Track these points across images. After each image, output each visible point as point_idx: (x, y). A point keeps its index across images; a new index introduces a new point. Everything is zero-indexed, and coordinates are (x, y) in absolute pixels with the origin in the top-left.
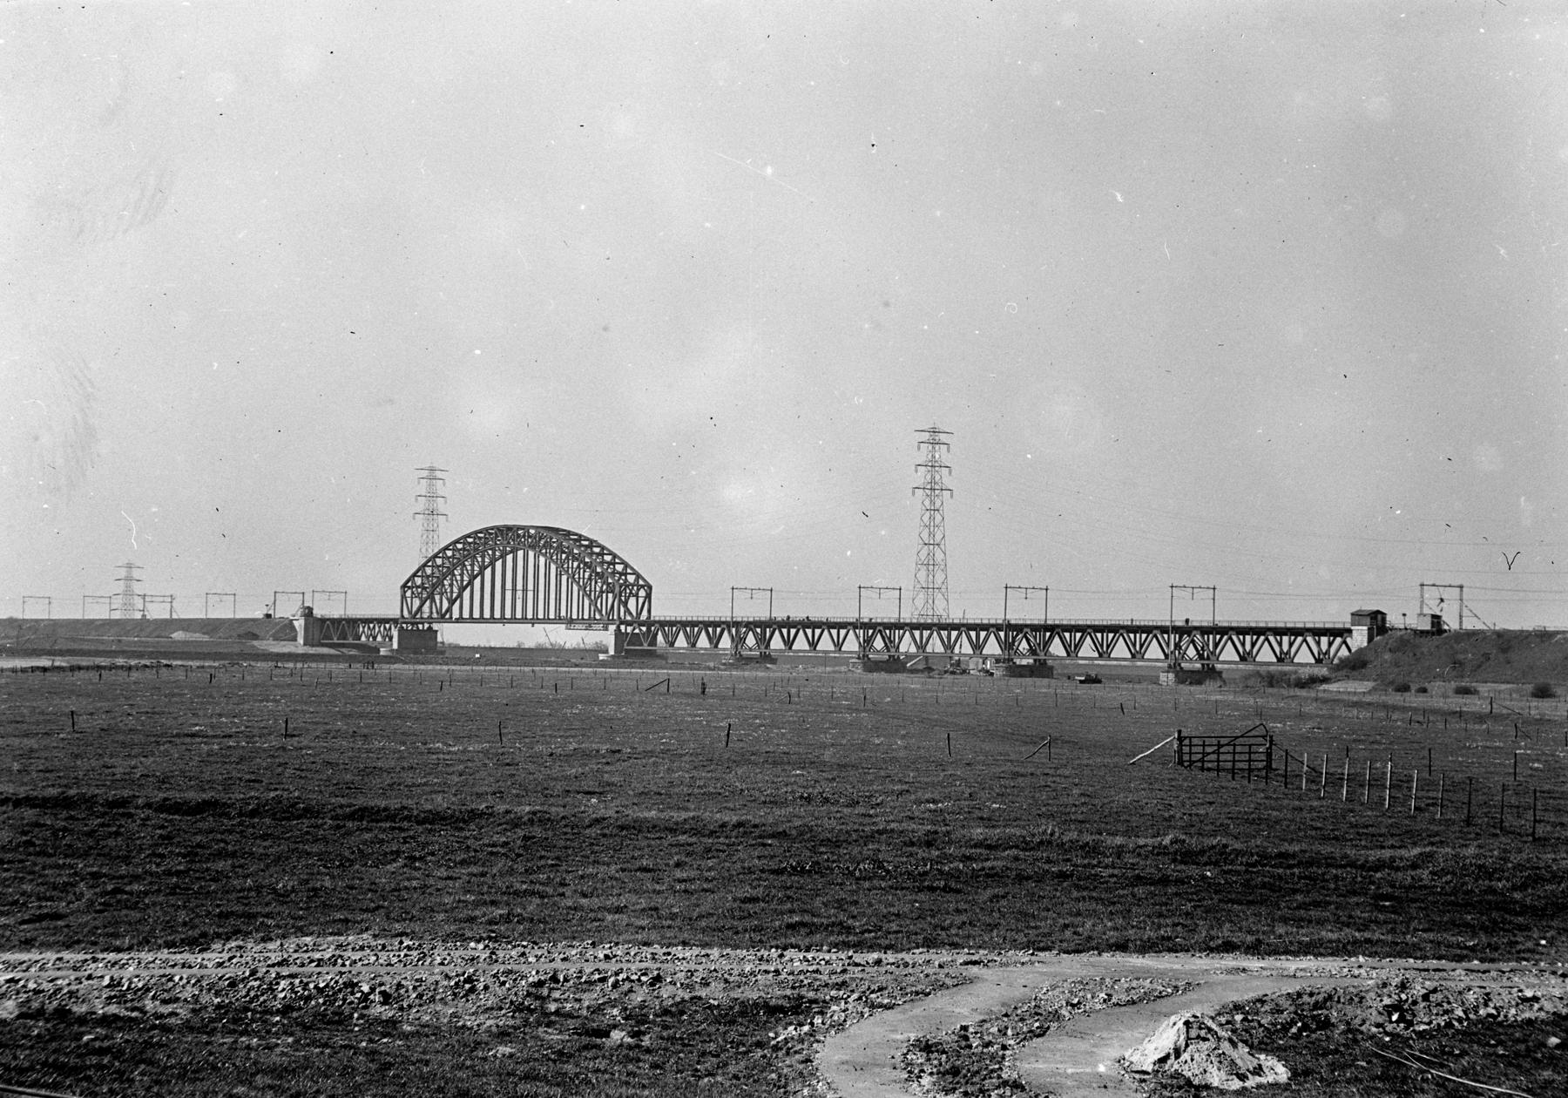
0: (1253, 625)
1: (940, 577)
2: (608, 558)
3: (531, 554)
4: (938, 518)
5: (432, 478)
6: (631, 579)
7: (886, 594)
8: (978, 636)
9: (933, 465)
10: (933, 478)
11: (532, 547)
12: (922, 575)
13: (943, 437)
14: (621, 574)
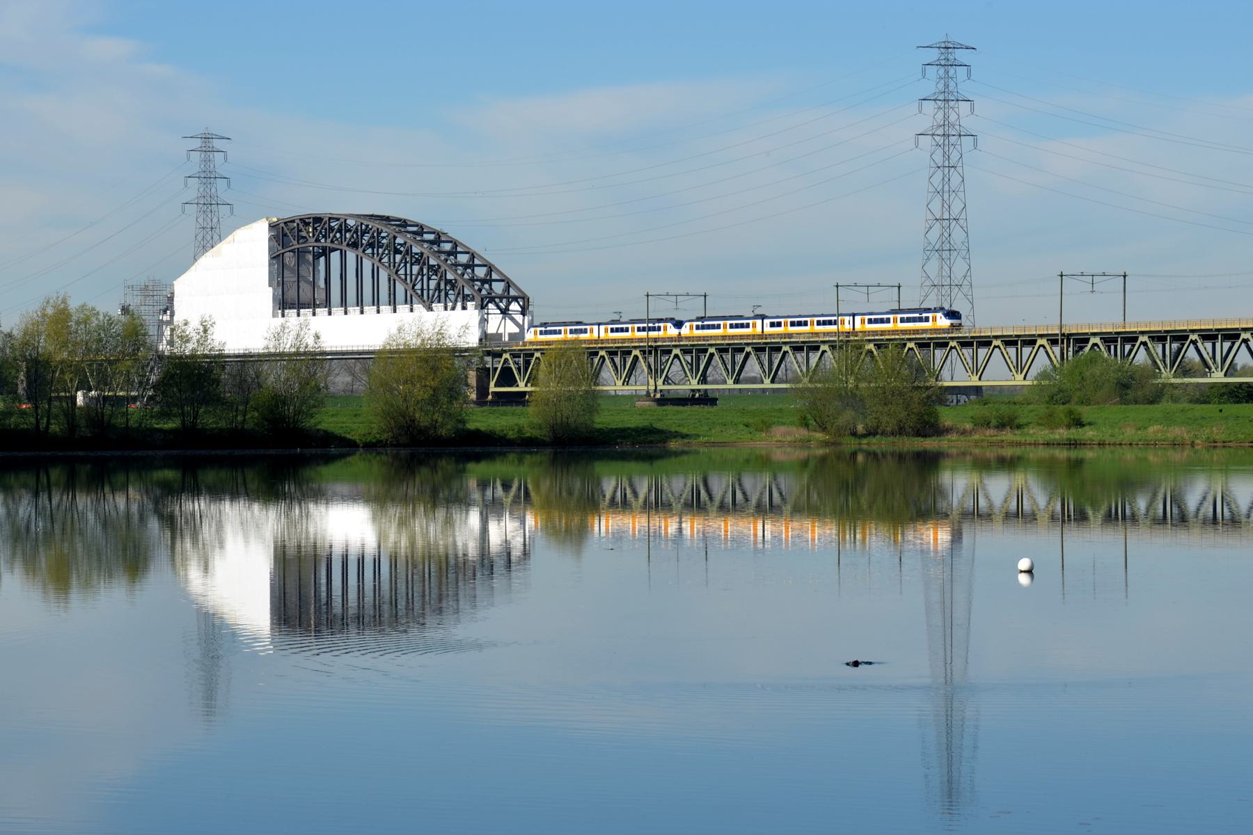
0: (355, 349)
1: (959, 268)
2: (463, 259)
3: (351, 256)
4: (955, 179)
5: (948, 64)
6: (498, 288)
7: (1102, 285)
8: (975, 357)
9: (946, 98)
10: (946, 117)
11: (354, 245)
12: (933, 267)
13: (960, 55)
14: (483, 281)
